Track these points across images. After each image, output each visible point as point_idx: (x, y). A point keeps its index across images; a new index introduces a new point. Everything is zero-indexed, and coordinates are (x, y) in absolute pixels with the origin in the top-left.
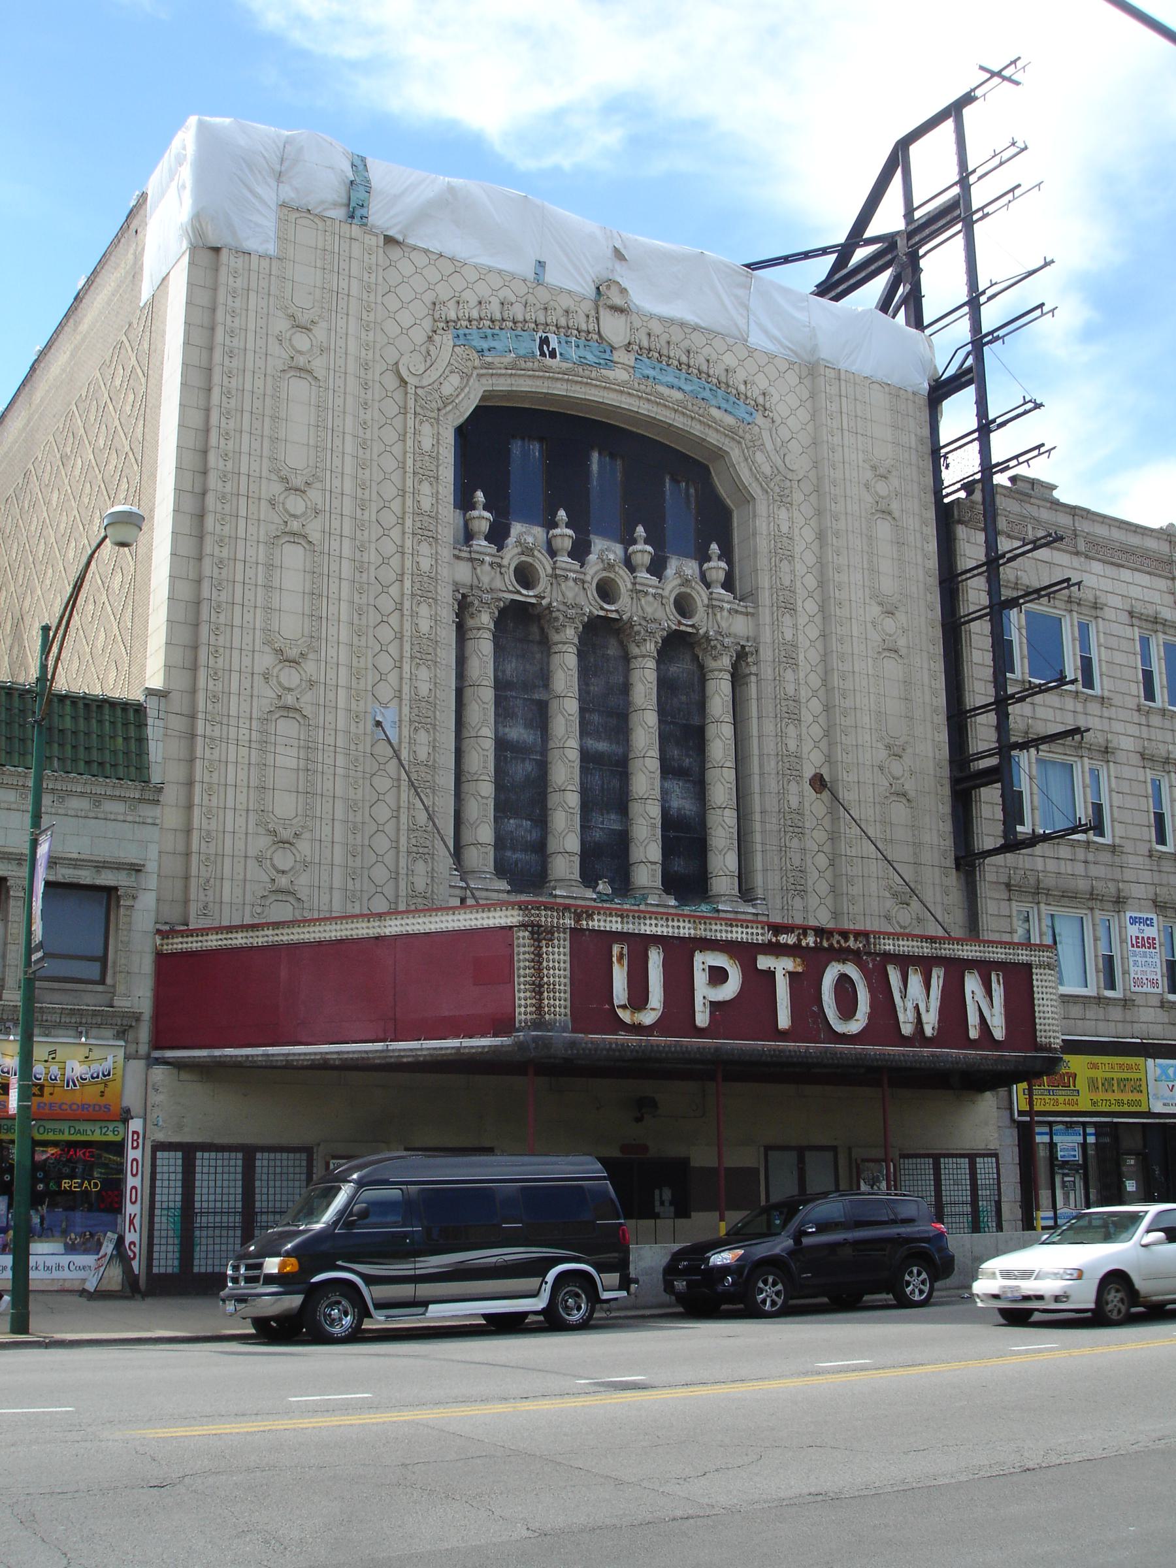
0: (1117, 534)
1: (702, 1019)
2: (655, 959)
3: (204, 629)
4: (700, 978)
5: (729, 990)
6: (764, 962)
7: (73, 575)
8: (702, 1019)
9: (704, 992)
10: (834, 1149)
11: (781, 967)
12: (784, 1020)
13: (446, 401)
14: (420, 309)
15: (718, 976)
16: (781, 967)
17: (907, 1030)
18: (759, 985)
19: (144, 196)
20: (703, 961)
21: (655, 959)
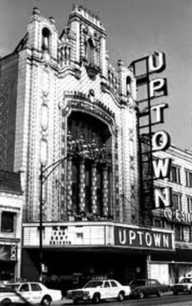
0: (177, 175)
1: (131, 243)
2: (125, 232)
3: (30, 140)
4: (130, 235)
5: (134, 238)
6: (138, 232)
7: (176, 146)
8: (131, 243)
9: (131, 238)
10: (23, 228)
11: (140, 233)
12: (141, 243)
13: (67, 112)
14: (62, 92)
15: (132, 235)
16: (140, 233)
17: (165, 246)
18: (138, 235)
19: (28, 33)
20: (131, 232)
21: (125, 232)
